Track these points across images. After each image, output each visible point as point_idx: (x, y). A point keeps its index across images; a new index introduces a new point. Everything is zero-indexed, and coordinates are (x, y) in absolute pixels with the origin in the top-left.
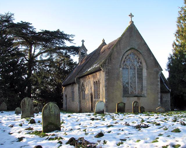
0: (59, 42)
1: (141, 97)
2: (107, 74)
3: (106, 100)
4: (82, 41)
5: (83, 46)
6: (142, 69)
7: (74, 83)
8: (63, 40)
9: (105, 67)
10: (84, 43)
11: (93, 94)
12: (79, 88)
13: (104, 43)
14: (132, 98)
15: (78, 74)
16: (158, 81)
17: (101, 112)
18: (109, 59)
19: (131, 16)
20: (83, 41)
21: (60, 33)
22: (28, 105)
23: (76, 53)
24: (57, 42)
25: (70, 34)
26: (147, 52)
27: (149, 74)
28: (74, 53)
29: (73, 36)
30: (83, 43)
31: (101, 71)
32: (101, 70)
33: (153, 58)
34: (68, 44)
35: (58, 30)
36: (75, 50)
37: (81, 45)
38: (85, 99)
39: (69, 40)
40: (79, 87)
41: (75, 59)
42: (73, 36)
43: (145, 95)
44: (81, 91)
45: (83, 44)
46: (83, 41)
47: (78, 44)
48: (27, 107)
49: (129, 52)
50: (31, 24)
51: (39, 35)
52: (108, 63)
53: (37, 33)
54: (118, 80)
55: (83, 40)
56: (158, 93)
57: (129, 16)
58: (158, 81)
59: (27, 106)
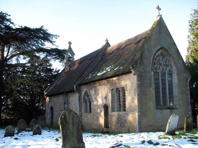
0: (37, 44)
1: (174, 109)
2: (139, 79)
3: (139, 113)
4: (69, 43)
5: (70, 48)
6: (172, 74)
7: (72, 91)
8: (42, 41)
9: (137, 68)
10: (71, 45)
11: (110, 106)
12: (80, 98)
13: (108, 44)
14: (165, 110)
15: (78, 80)
16: (188, 89)
17: (172, 133)
18: (141, 58)
19: (159, 8)
20: (70, 43)
21: (43, 31)
22: (73, 124)
23: (58, 58)
24: (35, 43)
25: (54, 35)
26: (176, 54)
27: (179, 80)
28: (55, 58)
29: (57, 37)
30: (70, 45)
31: (132, 75)
32: (131, 72)
33: (182, 62)
34: (48, 45)
35: (42, 27)
36: (59, 54)
37: (67, 48)
38: (91, 112)
39: (51, 42)
40: (79, 97)
41: (57, 65)
42: (57, 37)
43: (177, 106)
44: (82, 102)
45: (70, 47)
46: (70, 43)
47: (62, 45)
48: (71, 129)
49: (159, 52)
50: (10, 15)
51: (16, 32)
52: (140, 64)
53: (14, 30)
54: (150, 87)
55: (70, 42)
56: (188, 104)
57: (157, 8)
58: (188, 91)
59: (71, 126)
